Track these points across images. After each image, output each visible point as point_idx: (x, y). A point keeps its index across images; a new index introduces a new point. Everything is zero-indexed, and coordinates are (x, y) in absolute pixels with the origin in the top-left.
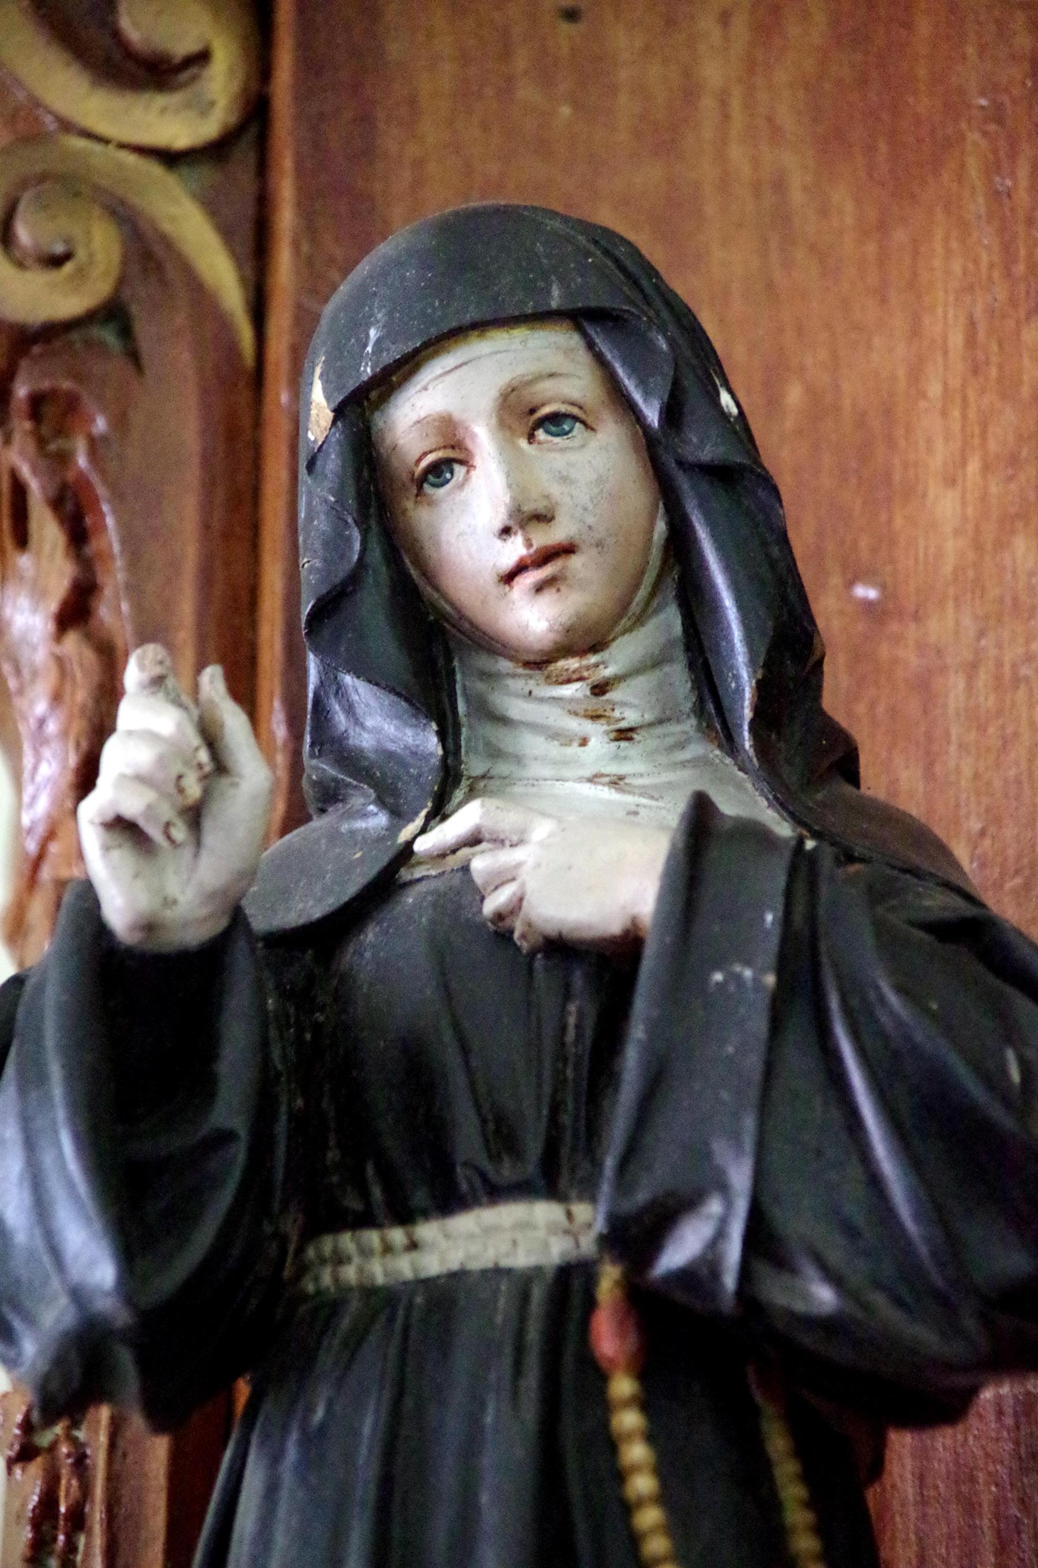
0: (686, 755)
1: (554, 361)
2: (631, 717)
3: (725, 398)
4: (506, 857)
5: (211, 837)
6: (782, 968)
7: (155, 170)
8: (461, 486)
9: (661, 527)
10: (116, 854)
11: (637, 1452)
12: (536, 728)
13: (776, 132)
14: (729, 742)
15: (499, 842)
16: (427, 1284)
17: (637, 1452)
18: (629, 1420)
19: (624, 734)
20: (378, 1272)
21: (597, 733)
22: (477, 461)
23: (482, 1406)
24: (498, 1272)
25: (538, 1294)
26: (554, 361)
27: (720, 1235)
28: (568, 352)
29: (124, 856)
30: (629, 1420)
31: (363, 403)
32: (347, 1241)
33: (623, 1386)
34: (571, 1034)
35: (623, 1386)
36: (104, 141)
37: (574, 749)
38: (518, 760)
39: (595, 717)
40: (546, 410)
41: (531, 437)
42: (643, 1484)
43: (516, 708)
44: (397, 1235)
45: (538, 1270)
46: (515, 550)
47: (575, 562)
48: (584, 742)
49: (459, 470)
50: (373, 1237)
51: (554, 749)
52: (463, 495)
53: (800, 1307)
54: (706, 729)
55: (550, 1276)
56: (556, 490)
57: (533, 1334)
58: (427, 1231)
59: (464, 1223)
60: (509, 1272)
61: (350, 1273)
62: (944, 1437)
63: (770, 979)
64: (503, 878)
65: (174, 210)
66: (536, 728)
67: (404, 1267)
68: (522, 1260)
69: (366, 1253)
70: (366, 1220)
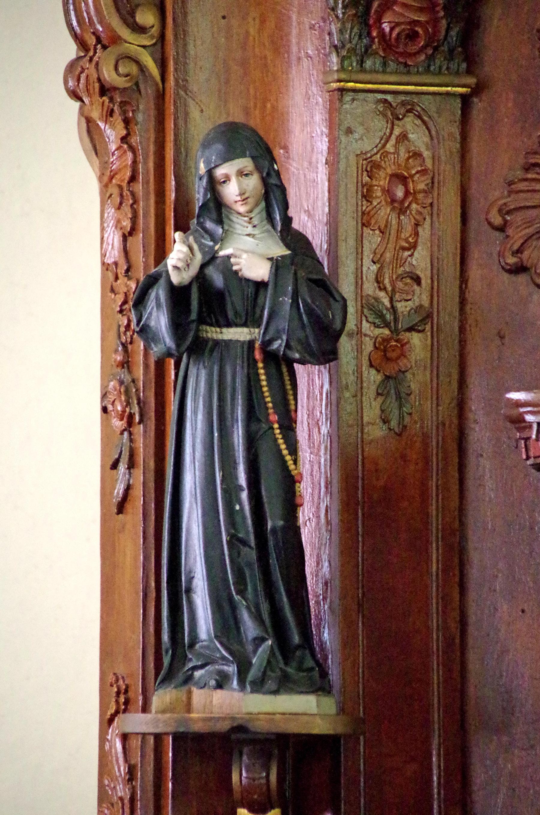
0: (265, 228)
1: (246, 164)
2: (256, 223)
3: (275, 166)
4: (237, 260)
5: (191, 267)
6: (292, 299)
7: (142, 49)
8: (228, 184)
9: (263, 191)
10: (175, 271)
11: (263, 377)
12: (238, 223)
13: (264, 45)
14: (274, 226)
15: (236, 257)
16: (225, 341)
17: (263, 377)
18: (262, 371)
19: (254, 226)
20: (215, 336)
21: (250, 226)
22: (231, 180)
23: (236, 368)
24: (238, 341)
25: (246, 347)
26: (246, 164)
27: (280, 345)
28: (248, 161)
29: (176, 272)
30: (262, 371)
31: (283, 354)
32: (208, 328)
33: (260, 365)
34: (250, 295)
35: (260, 365)
36: (133, 44)
37: (245, 229)
38: (234, 228)
39: (250, 223)
40: (245, 173)
41: (241, 177)
42: (264, 383)
43: (234, 219)
44: (218, 330)
45: (245, 341)
46: (239, 198)
47: (249, 200)
48: (247, 227)
49: (228, 182)
50: (213, 329)
51: (242, 228)
52: (228, 186)
53: (294, 357)
54: (269, 227)
55: (247, 343)
56: (246, 188)
57: (245, 356)
58: (224, 330)
59: (232, 330)
60: (240, 341)
61: (209, 335)
62: (241, 174)
63: (290, 301)
64: (238, 264)
65: (146, 59)
66: (238, 223)
67: (220, 337)
68: (242, 339)
69: (212, 332)
70: (211, 325)
